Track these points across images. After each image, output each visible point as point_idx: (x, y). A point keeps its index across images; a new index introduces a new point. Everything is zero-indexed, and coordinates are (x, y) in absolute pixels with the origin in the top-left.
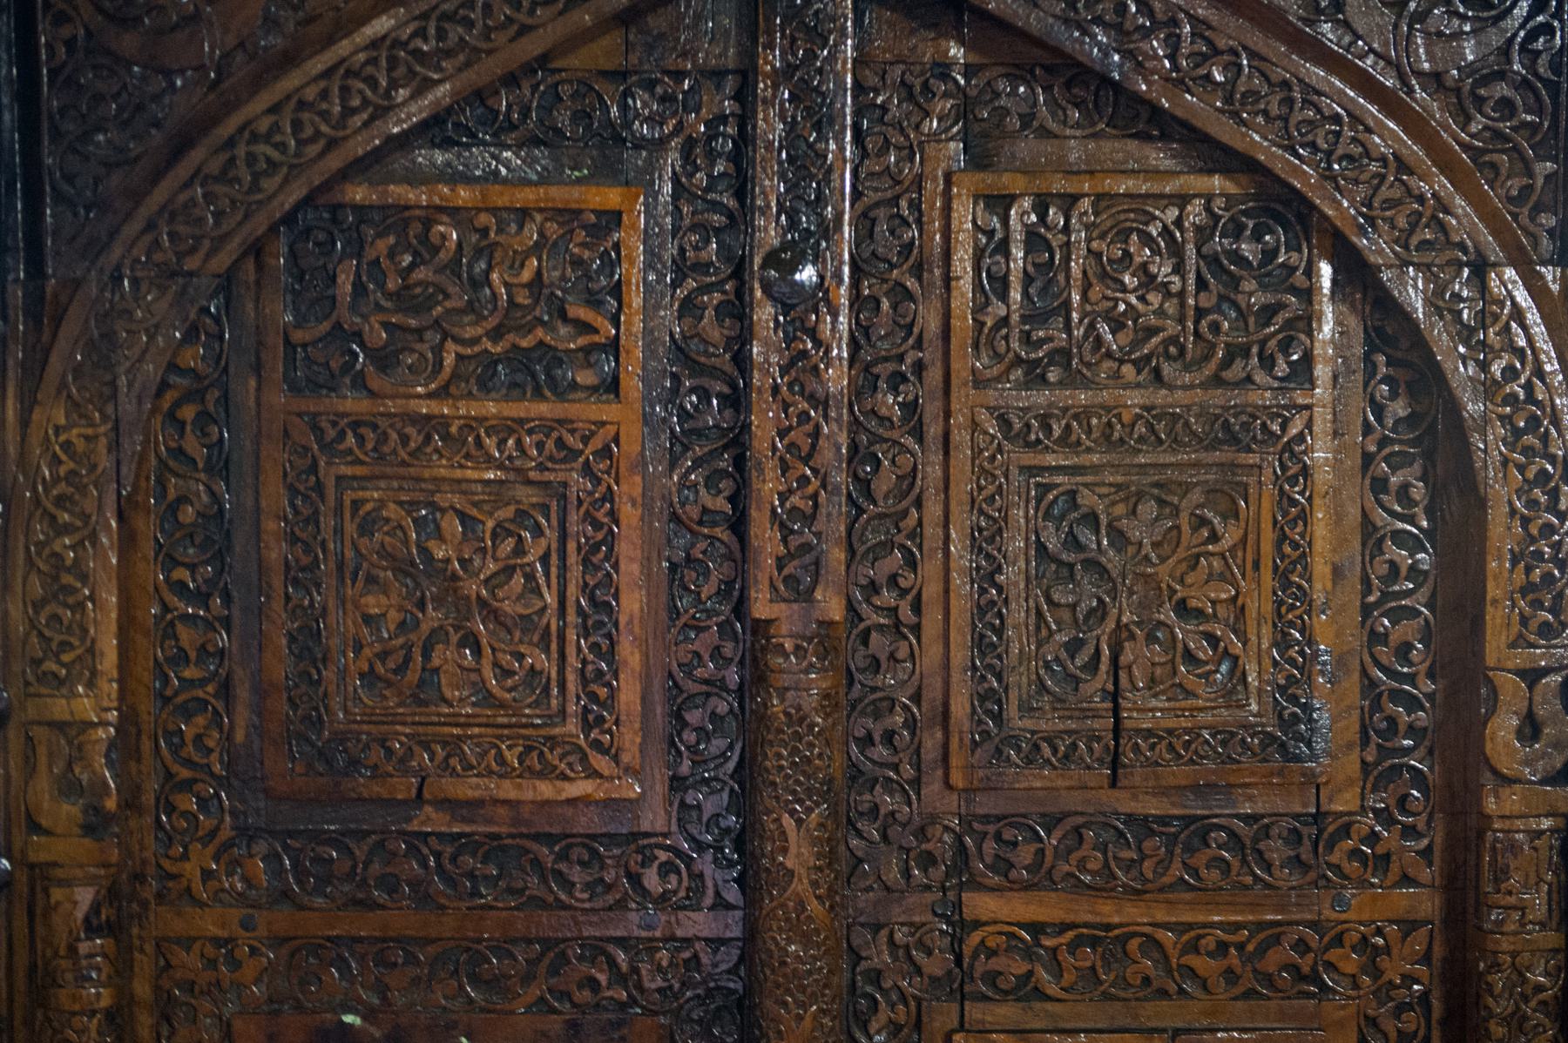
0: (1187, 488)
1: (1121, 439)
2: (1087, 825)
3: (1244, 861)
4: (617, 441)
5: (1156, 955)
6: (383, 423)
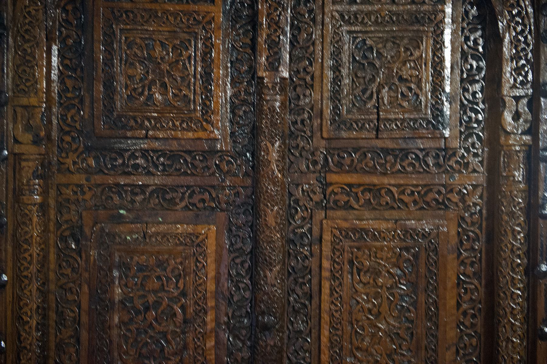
0: (402, 38)
1: (381, 22)
2: (368, 152)
3: (420, 164)
5: (391, 195)
6: (136, 11)
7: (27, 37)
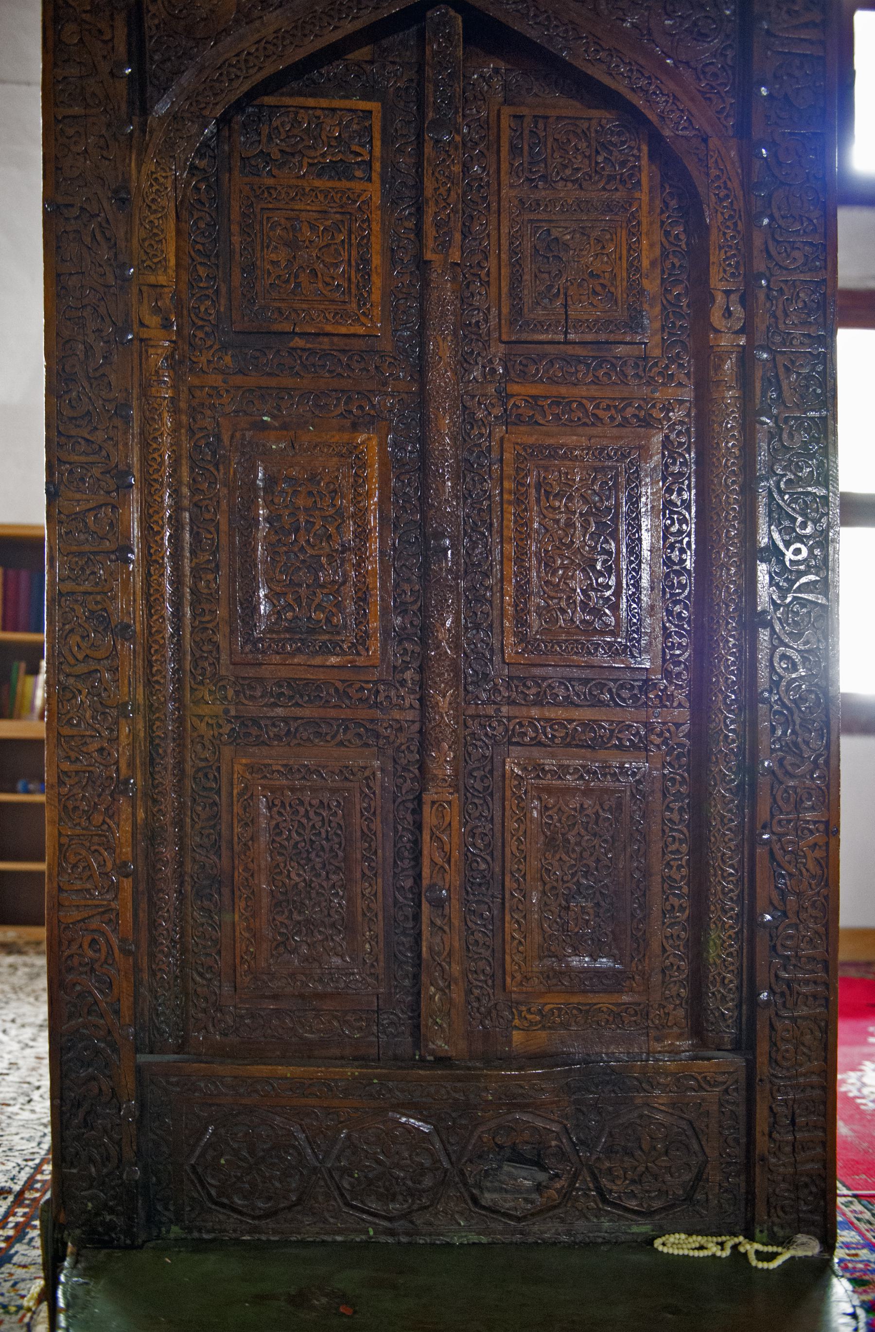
4: (371, 198)
7: (154, 207)
